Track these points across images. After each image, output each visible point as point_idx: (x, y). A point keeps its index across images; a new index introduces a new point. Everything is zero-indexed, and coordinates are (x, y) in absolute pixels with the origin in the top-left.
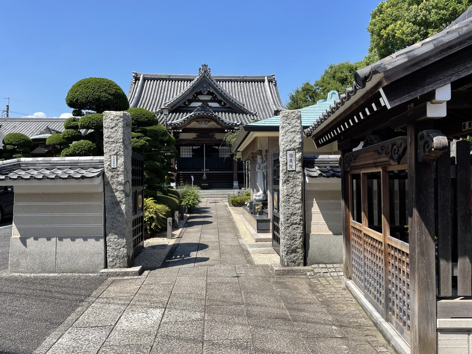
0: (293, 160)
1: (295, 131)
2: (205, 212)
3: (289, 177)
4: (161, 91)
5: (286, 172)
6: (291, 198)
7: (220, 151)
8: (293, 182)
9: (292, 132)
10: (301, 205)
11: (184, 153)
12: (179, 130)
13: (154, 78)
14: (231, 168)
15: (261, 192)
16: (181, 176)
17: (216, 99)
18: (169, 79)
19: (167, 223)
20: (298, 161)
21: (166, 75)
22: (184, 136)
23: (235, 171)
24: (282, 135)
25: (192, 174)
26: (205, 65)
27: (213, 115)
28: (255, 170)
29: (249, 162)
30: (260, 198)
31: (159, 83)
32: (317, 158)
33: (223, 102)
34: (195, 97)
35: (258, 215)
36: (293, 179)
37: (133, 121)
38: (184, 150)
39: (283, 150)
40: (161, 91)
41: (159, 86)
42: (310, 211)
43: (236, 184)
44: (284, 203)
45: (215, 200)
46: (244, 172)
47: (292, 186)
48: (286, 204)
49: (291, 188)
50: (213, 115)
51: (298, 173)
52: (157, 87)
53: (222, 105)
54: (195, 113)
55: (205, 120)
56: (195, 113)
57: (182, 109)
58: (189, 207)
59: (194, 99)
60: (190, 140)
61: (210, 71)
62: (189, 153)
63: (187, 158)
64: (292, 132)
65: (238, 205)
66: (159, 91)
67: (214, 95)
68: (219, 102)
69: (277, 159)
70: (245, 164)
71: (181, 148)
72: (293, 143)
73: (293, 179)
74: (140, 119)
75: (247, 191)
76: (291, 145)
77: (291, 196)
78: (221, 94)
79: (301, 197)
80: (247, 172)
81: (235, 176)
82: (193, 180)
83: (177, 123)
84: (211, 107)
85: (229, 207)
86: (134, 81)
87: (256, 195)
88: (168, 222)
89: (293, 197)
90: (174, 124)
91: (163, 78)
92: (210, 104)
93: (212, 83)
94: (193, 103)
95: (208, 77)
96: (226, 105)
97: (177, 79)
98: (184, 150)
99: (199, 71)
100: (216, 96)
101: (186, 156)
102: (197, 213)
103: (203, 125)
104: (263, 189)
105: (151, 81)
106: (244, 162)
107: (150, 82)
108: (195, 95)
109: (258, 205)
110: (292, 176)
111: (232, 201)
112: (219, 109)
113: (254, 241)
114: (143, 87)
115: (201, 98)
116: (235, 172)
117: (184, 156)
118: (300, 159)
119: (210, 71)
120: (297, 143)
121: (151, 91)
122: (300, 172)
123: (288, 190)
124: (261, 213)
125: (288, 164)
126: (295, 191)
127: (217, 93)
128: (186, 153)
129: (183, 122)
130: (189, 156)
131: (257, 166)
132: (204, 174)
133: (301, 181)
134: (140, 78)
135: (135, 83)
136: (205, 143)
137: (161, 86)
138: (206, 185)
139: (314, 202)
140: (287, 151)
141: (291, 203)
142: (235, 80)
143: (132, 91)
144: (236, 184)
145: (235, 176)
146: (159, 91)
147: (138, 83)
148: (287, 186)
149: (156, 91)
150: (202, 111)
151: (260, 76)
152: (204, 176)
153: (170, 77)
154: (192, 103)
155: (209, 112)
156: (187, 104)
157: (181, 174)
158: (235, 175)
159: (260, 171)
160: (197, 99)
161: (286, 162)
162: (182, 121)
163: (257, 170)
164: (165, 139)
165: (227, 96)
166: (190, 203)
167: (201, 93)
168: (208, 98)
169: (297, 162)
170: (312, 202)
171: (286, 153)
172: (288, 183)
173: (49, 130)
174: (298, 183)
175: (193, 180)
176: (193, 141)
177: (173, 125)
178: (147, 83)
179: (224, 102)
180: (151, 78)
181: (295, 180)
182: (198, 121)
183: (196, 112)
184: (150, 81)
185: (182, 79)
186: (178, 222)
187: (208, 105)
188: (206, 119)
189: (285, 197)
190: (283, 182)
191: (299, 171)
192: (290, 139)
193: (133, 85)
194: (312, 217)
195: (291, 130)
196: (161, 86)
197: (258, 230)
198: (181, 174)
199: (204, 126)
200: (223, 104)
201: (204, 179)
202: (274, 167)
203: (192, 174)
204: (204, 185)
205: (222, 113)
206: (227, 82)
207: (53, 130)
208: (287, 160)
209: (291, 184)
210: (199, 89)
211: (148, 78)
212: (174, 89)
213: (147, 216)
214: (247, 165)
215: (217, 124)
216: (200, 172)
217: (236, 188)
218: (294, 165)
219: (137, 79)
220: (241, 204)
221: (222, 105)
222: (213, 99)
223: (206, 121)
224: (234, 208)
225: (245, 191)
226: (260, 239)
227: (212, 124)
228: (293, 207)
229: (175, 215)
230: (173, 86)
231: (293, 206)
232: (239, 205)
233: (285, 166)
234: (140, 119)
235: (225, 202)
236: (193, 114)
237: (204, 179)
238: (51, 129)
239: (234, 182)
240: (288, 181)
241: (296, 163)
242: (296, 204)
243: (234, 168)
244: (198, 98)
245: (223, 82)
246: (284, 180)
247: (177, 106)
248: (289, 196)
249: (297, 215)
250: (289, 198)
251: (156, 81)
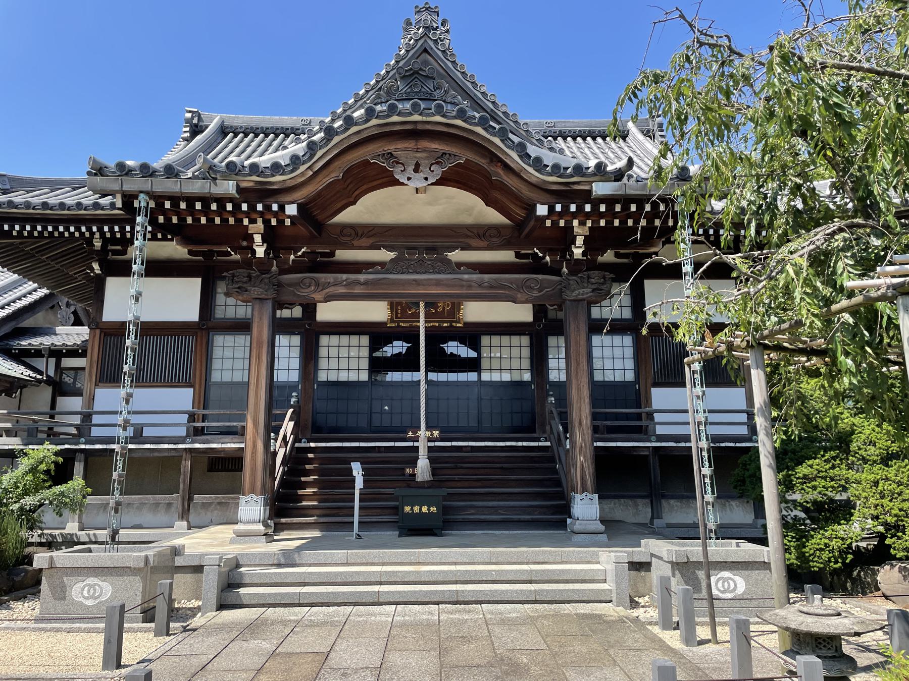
11: (333, 364)
16: (310, 461)
55: (424, 150)
71: (324, 340)
82: (359, 483)
86: (188, 135)
98: (334, 352)
99: (406, 30)
101: (343, 377)
117: (333, 377)
130: (353, 377)
132: (423, 452)
138: (425, 509)
157: (311, 456)
158: (580, 459)
175: (359, 483)
198: (311, 456)
201: (419, 478)
204: (416, 509)
237: (419, 478)
243: (576, 423)
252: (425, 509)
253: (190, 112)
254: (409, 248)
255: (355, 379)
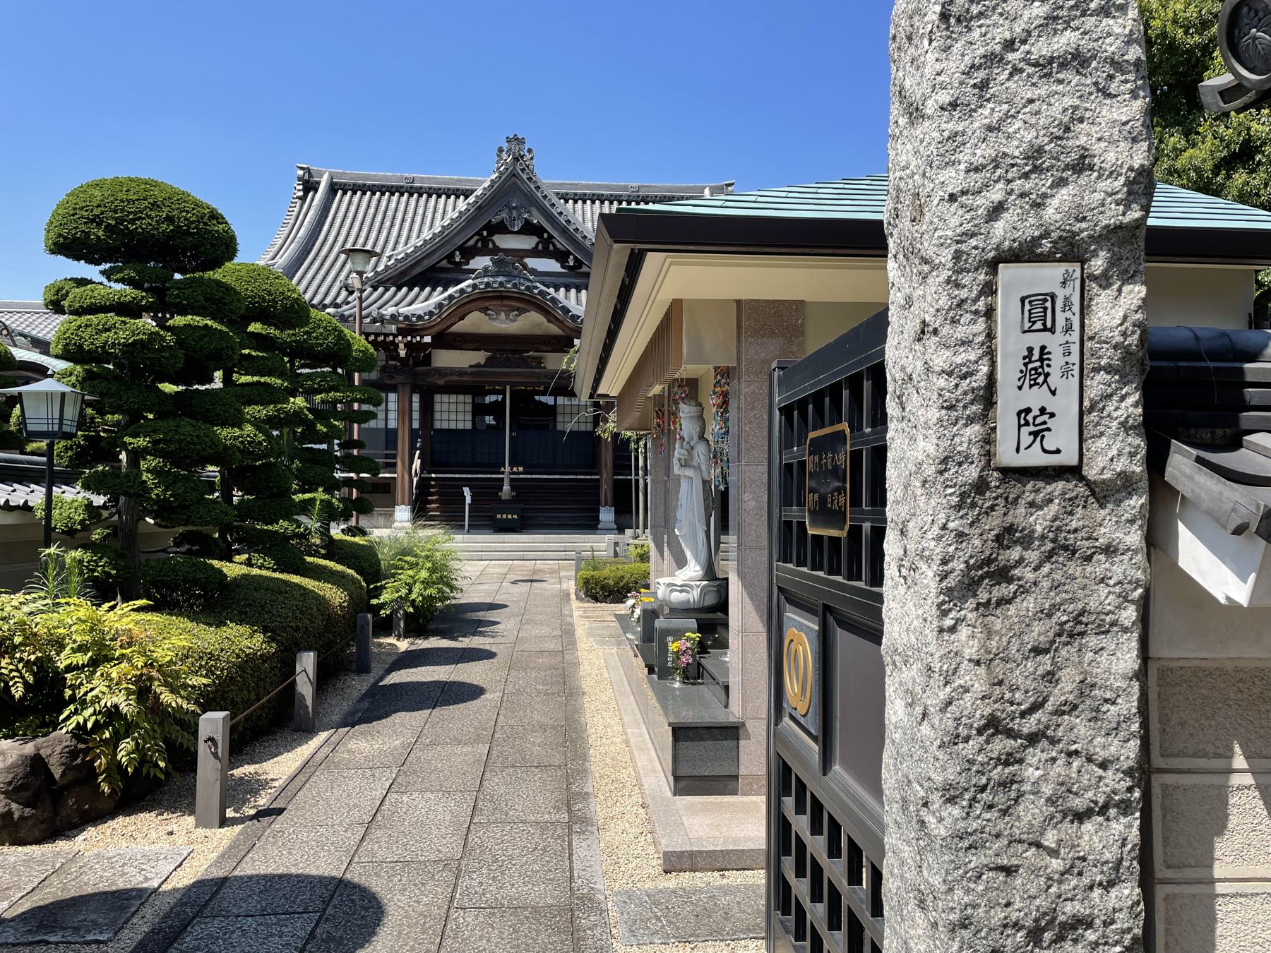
0: (1057, 360)
1: (1078, 60)
2: (476, 627)
3: (1008, 535)
4: (382, 223)
5: (981, 486)
6: (1035, 755)
7: (560, 410)
8: (1055, 587)
9: (1046, 67)
10: (1134, 835)
11: (445, 416)
12: (422, 337)
13: (364, 185)
14: (593, 464)
15: (693, 570)
16: (433, 487)
17: (551, 247)
18: (412, 190)
19: (197, 739)
20: (1109, 369)
21: (401, 177)
22: (446, 359)
23: (605, 476)
24: (944, 97)
25: (467, 482)
26: (516, 139)
27: (536, 291)
28: (668, 468)
29: (649, 445)
30: (690, 596)
31: (379, 201)
32: (1254, 357)
33: (571, 257)
34: (485, 241)
35: (677, 685)
36: (1049, 556)
37: (101, 233)
38: (445, 407)
39: (957, 256)
40: (382, 223)
41: (377, 209)
42: (1190, 873)
43: (607, 515)
44: (956, 811)
45: (535, 571)
46: (633, 477)
47: (1037, 628)
48: (982, 819)
49: (1037, 651)
50: (536, 291)
51: (1103, 493)
52: (372, 211)
53: (570, 268)
54: (476, 281)
55: (506, 306)
56: (476, 281)
57: (443, 275)
58: (411, 610)
59: (479, 245)
60: (461, 372)
61: (532, 159)
62: (460, 417)
63: (457, 431)
64: (1046, 67)
65: (606, 597)
66: (377, 224)
67: (546, 235)
68: (561, 256)
69: (855, 383)
70: (637, 450)
71: (438, 398)
72: (1061, 183)
73: (1049, 556)
74: (132, 222)
75: (641, 542)
76: (1037, 205)
77: (1033, 739)
78: (564, 232)
79: (1134, 744)
80: (643, 478)
81: (606, 489)
82: (468, 500)
83: (413, 315)
84: (533, 271)
85: (575, 604)
86: (301, 194)
87: (669, 585)
88: (203, 735)
89: (1053, 741)
90: (406, 318)
91: (392, 186)
92: (532, 262)
93: (539, 194)
94: (477, 258)
95: (525, 177)
96: (581, 268)
97: (435, 189)
98: (445, 407)
99: (499, 156)
100: (551, 237)
101: (453, 426)
102: (444, 634)
103: (502, 322)
104: (703, 555)
105: (354, 193)
106: (633, 445)
107: (352, 197)
108: (485, 233)
109: (678, 634)
110: (1039, 522)
111: (587, 582)
112: (561, 280)
113: (656, 863)
114: (328, 212)
115: (506, 242)
116: (606, 478)
117: (445, 426)
118: (1127, 353)
119: (532, 159)
120: (1106, 185)
121: (352, 224)
122: (1125, 485)
123: (999, 669)
124: (694, 674)
125: (1009, 400)
126: (1067, 686)
127: (553, 227)
128: (460, 417)
129: (436, 311)
130: (460, 426)
131: (679, 452)
132: (506, 482)
133: (1137, 584)
134: (319, 183)
135: (303, 199)
136: (512, 385)
137: (382, 208)
138: (510, 516)
139: (1236, 780)
140: (993, 266)
141: (1030, 812)
142: (611, 195)
143: (292, 221)
144: (607, 515)
145: (606, 489)
146: (377, 224)
147: (312, 200)
148: (990, 634)
149: (368, 221)
150: (498, 276)
151: (687, 188)
152: (506, 488)
153: (413, 182)
154: (473, 258)
155: (522, 281)
156: (457, 259)
157: (433, 483)
159: (689, 472)
160: (491, 245)
161: (979, 380)
162: (431, 309)
163: (676, 469)
164: (321, 345)
165: (585, 237)
166: (413, 596)
167: (502, 228)
168: (528, 243)
169: (1097, 385)
170: (1216, 780)
171: (989, 289)
172: (1004, 601)
173: (9, 333)
174: (1103, 597)
175: (468, 500)
176: (472, 374)
177: (401, 318)
178: (341, 201)
179: (575, 257)
180: (354, 185)
181: (1074, 568)
182: (484, 310)
183: (479, 280)
184: (349, 193)
185: (449, 189)
186: (309, 702)
187: (525, 266)
188: (513, 303)
189: (969, 749)
190: (949, 591)
191: (1123, 475)
192: (1029, 136)
193: (298, 205)
194: (1219, 930)
195: (1041, 48)
196: (382, 208)
197: (677, 778)
198: (433, 483)
199: (504, 326)
200: (571, 263)
202: (786, 444)
203: (467, 482)
204: (504, 516)
205: (568, 290)
206: (588, 202)
207: (21, 335)
208: (991, 354)
209: (1029, 604)
210: (497, 214)
211: (345, 184)
212: (406, 207)
213: (97, 699)
214: (643, 454)
215: (549, 321)
216: (494, 476)
217: (608, 530)
218: (1066, 405)
219: (309, 186)
220: (618, 591)
221: (570, 268)
222: (540, 247)
223: (513, 309)
224: (591, 605)
225: (636, 542)
226: (692, 855)
227: (530, 322)
228: (1054, 853)
229: (298, 669)
230: (421, 210)
231: (1050, 839)
232: (609, 596)
233: (971, 420)
234: (132, 222)
235: (565, 577)
236: (468, 287)
238: (13, 331)
239: (602, 509)
240: (1003, 575)
241: (1093, 392)
242: (1081, 817)
243: (603, 465)
244: (494, 243)
245: (575, 202)
246: (958, 566)
247: (427, 264)
248: (1011, 734)
249: (1091, 936)
250: (1008, 760)
251: (369, 193)
252: (510, 516)
253: (302, 168)
254: (500, 350)
255: (444, 396)
